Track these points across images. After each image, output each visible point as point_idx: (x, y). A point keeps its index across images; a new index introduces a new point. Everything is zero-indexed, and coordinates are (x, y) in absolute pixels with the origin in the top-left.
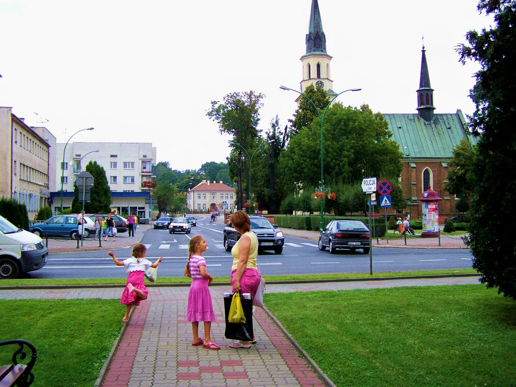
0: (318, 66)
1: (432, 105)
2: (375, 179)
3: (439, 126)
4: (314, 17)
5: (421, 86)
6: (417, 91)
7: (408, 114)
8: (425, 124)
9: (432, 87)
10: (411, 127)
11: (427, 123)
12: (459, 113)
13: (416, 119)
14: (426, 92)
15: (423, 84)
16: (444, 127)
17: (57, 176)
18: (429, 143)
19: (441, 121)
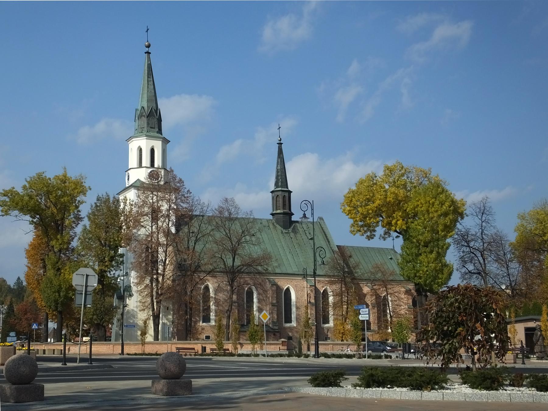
0: (152, 151)
1: (290, 209)
2: (509, 326)
3: (298, 235)
4: (148, 87)
5: (276, 185)
6: (272, 192)
7: (261, 219)
8: (282, 233)
9: (290, 188)
10: (266, 236)
11: (284, 231)
12: (321, 222)
13: (271, 226)
14: (284, 194)
15: (280, 184)
16: (304, 237)
17: (538, 366)
18: (289, 257)
19: (300, 230)
